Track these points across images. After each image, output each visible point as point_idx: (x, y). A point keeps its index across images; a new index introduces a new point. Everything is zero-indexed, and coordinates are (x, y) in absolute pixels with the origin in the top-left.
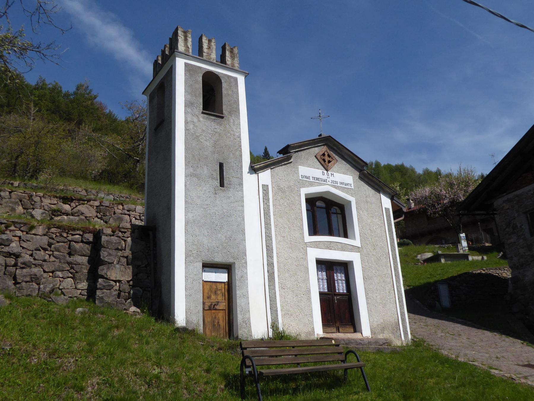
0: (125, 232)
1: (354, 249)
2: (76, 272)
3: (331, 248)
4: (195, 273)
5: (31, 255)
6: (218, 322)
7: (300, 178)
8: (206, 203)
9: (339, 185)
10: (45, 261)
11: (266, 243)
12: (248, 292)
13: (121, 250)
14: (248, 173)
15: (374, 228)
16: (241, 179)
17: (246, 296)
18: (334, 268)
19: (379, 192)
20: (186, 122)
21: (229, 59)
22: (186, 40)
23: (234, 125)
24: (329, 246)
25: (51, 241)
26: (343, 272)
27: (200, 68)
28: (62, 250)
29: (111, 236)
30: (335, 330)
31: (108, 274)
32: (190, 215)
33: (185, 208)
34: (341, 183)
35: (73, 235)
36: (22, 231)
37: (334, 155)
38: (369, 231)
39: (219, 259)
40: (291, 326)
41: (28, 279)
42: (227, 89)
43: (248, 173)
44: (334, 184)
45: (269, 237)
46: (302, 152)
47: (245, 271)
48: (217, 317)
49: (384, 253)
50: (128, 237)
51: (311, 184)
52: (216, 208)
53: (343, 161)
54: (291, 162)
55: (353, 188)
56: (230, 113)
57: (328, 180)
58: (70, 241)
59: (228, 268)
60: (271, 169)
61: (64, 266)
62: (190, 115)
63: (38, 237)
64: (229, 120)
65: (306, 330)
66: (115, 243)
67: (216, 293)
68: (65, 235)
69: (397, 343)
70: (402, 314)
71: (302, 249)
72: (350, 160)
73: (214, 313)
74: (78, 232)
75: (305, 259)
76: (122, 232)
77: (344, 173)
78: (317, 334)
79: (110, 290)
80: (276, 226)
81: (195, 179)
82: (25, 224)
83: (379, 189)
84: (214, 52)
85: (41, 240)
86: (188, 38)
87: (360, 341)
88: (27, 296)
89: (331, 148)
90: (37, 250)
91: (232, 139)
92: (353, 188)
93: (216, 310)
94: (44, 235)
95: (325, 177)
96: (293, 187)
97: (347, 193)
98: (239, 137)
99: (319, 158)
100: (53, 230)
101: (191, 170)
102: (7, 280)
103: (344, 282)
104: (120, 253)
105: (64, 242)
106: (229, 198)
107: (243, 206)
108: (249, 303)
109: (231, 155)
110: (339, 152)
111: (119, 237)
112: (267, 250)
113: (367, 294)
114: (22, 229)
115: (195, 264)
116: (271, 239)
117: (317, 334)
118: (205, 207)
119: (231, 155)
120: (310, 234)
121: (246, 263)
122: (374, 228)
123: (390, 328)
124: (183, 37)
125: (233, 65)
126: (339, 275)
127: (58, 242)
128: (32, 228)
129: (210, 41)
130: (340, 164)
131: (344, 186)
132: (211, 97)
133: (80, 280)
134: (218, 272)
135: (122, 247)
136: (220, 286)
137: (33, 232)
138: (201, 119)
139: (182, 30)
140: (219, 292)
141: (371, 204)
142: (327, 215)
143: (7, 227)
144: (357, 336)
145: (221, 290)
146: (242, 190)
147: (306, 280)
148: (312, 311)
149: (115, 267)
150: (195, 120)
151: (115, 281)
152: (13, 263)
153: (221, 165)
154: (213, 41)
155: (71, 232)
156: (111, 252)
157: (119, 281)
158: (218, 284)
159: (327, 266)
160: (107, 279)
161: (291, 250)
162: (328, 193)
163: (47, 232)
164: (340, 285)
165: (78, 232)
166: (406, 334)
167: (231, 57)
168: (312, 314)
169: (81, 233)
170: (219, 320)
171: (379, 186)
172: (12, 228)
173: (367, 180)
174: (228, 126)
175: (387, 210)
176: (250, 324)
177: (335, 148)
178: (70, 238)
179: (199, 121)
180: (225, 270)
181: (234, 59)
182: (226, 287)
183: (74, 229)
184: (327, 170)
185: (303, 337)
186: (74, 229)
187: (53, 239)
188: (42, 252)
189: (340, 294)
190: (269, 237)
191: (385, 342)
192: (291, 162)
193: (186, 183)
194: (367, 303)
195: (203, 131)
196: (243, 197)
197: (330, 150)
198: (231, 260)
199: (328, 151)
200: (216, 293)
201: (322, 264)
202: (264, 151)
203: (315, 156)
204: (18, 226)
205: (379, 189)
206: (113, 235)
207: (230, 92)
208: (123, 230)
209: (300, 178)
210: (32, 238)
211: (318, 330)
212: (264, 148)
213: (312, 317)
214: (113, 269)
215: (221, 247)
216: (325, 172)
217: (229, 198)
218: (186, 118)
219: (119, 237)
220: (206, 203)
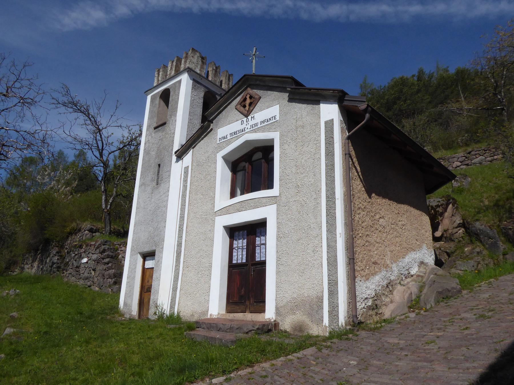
9: (259, 126)
22: (159, 74)
34: (263, 122)
44: (255, 129)
46: (224, 112)
51: (229, 142)
53: (269, 92)
72: (276, 85)
83: (318, 99)
98: (174, 133)
113: (278, 259)
117: (211, 315)
120: (270, 186)
122: (303, 161)
131: (266, 123)
173: (297, 97)
177: (258, 82)
184: (247, 116)
192: (212, 130)
201: (233, 231)
205: (318, 99)
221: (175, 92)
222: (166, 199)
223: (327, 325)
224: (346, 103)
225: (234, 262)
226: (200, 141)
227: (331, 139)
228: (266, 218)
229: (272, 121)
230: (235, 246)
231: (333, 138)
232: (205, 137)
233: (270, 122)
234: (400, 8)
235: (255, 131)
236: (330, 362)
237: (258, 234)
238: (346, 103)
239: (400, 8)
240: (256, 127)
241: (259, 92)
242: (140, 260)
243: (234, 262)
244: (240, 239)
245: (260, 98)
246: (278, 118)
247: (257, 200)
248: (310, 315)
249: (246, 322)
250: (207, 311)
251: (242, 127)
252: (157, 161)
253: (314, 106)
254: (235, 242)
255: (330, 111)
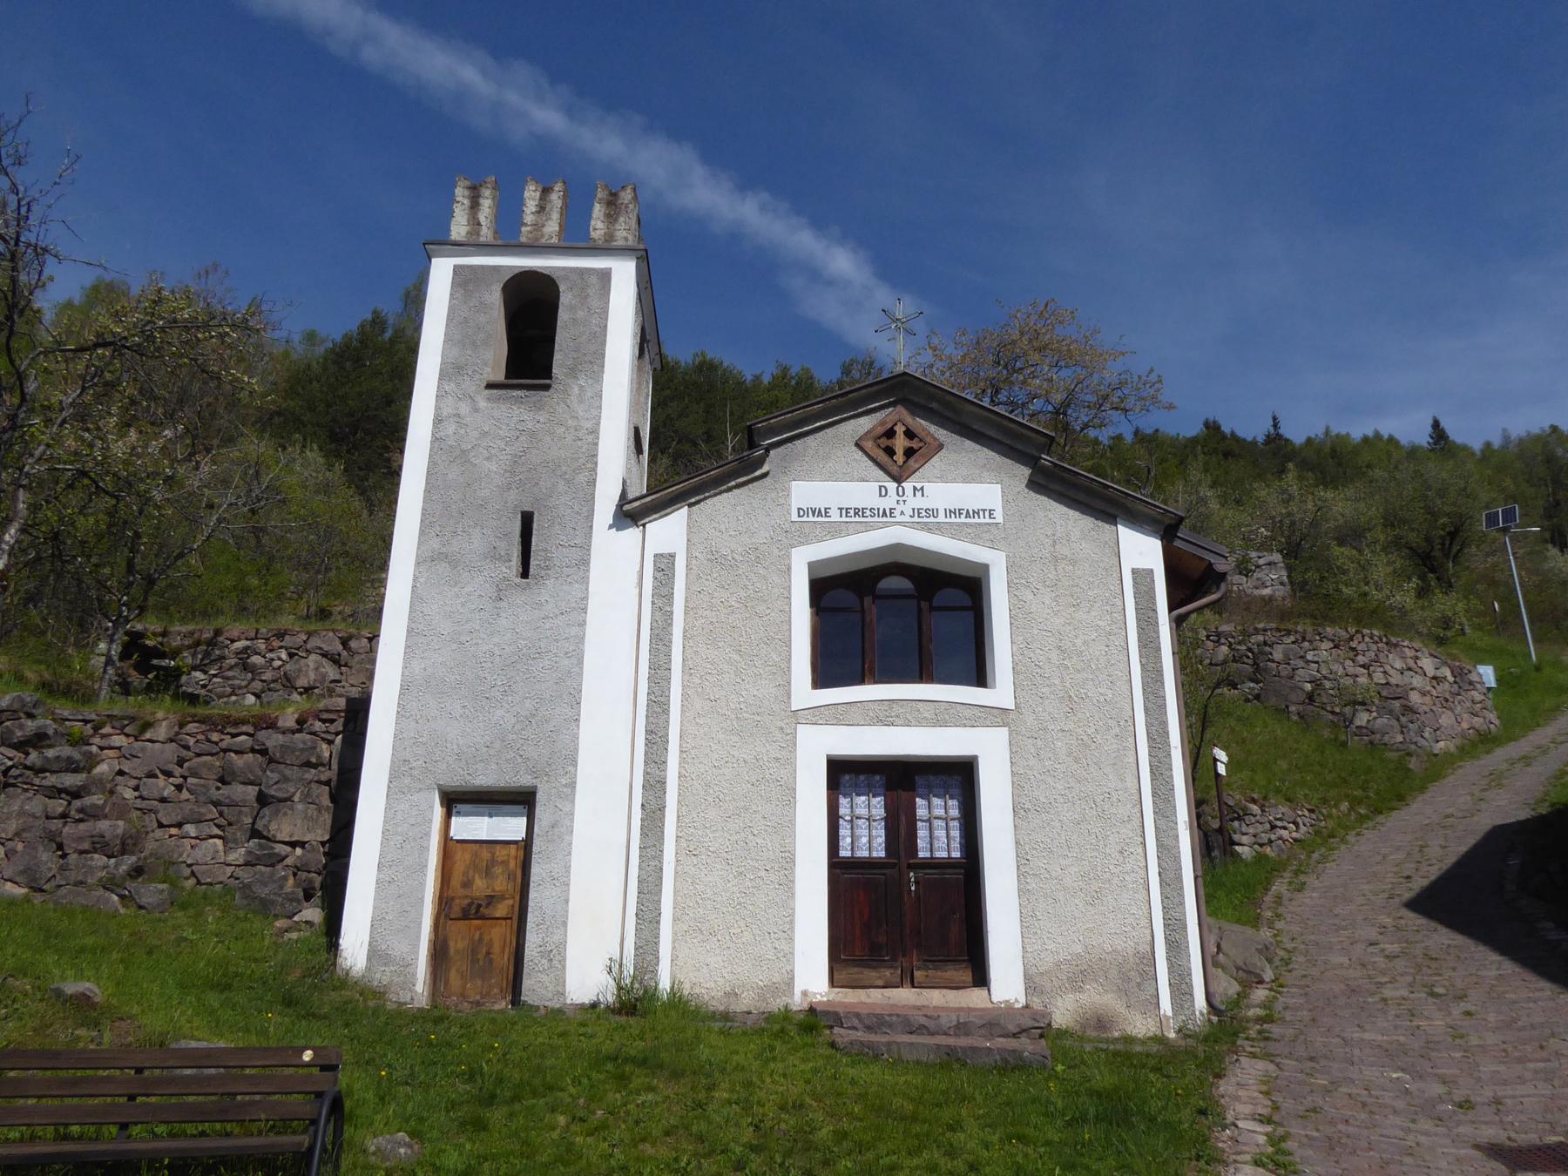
0: (332, 721)
1: (995, 716)
2: (230, 824)
3: (903, 720)
4: (412, 821)
5: (136, 789)
6: (488, 953)
7: (794, 517)
8: (467, 627)
9: (941, 518)
10: (163, 800)
11: (611, 728)
12: (568, 868)
13: (315, 766)
14: (611, 527)
15: (1079, 642)
16: (587, 548)
17: (562, 881)
18: (919, 780)
19: (1112, 519)
20: (438, 421)
21: (600, 225)
22: (475, 205)
23: (581, 402)
24: (885, 715)
25: (184, 753)
26: (957, 791)
27: (496, 269)
28: (204, 772)
29: (293, 732)
30: (967, 976)
31: (273, 826)
32: (417, 666)
33: (407, 647)
35: (234, 736)
36: (127, 735)
37: (933, 429)
38: (1054, 656)
39: (486, 778)
40: (689, 968)
41: (86, 846)
42: (572, 308)
43: (611, 527)
44: (925, 519)
45: (658, 706)
46: (810, 440)
47: (567, 809)
48: (486, 938)
49: (1112, 723)
50: (337, 734)
51: (835, 531)
52: (496, 640)
53: (968, 443)
54: (765, 475)
55: (999, 519)
56: (573, 372)
57: (900, 508)
58: (225, 751)
59: (523, 800)
60: (690, 505)
61: (202, 810)
62: (450, 400)
63: (157, 745)
64: (565, 392)
65: (761, 978)
66: (302, 750)
67: (488, 873)
68: (215, 737)
69: (1140, 1026)
70: (1174, 927)
71: (778, 735)
72: (992, 433)
73: (478, 928)
74: (244, 728)
75: (788, 760)
76: (324, 721)
77: (966, 480)
78: (805, 993)
79: (273, 865)
80: (687, 670)
81: (443, 567)
82: (133, 719)
83: (1112, 511)
84: (555, 216)
85: (162, 752)
86: (482, 201)
87: (923, 1021)
88: (75, 884)
89: (916, 409)
90: (152, 775)
91: (569, 438)
92: (999, 519)
93: (483, 918)
94: (172, 741)
95: (888, 503)
96: (762, 548)
97: (974, 540)
99: (869, 445)
100: (191, 728)
101: (435, 544)
102: (41, 848)
103: (956, 824)
104: (311, 774)
105: (212, 755)
106: (540, 604)
107: (583, 624)
108: (567, 901)
109: (561, 486)
110: (950, 415)
111: (314, 734)
112: (648, 742)
114: (127, 730)
115: (415, 798)
116: (666, 712)
117: (805, 993)
118: (463, 639)
119: (561, 486)
121: (572, 785)
122: (1079, 642)
123: (1113, 973)
124: (466, 202)
125: (610, 237)
126: (936, 801)
127: (199, 755)
128: (147, 726)
129: (546, 191)
130: (959, 451)
131: (963, 519)
132: (531, 336)
133: (235, 841)
134: (497, 815)
135: (319, 757)
136: (504, 852)
137: (148, 735)
138: (482, 404)
139: (467, 183)
140: (498, 870)
141: (1073, 562)
142: (899, 618)
143: (96, 729)
144: (973, 998)
145: (505, 863)
146: (585, 580)
147: (786, 827)
148: (792, 922)
149: (292, 808)
150: (464, 408)
151: (293, 845)
152: (60, 810)
153: (527, 520)
154: (558, 187)
155: (229, 730)
156: (288, 772)
157: (302, 844)
158: (498, 847)
159: (899, 779)
160: (268, 839)
161: (736, 738)
162: (897, 547)
163: (177, 734)
164: (940, 833)
165: (244, 728)
166: (1181, 989)
167: (608, 216)
168: (792, 929)
169: (250, 729)
170: (490, 945)
171: (1111, 501)
172: (107, 730)
173: (1057, 487)
174: (561, 408)
175: (1142, 578)
176: (563, 961)
177: (934, 405)
178: (228, 741)
179: (477, 410)
180: (519, 808)
181: (616, 220)
182: (521, 853)
183: (236, 723)
184: (898, 480)
185: (746, 1002)
186: (236, 723)
187: (187, 748)
188: (161, 780)
189: (933, 864)
190: (658, 706)
191: (1031, 1023)
192: (765, 475)
193: (415, 579)
194: (1022, 892)
195: (485, 434)
196: (585, 598)
197: (913, 414)
198: (525, 780)
199: (909, 420)
200: (488, 873)
201: (845, 774)
202: (1430, 430)
203: (857, 445)
204: (117, 724)
205: (1112, 511)
206: (300, 731)
207: (580, 314)
208: (325, 716)
209: (794, 517)
210: (143, 750)
211: (810, 976)
212: (1431, 422)
213: (791, 940)
214: (285, 814)
215: (498, 745)
216: (892, 486)
217: (540, 604)
218: (437, 408)
219: (314, 734)
220: (467, 627)
221: (584, 298)
222: (574, 631)
223: (1170, 1013)
224: (1177, 543)
225: (845, 853)
226: (720, 493)
227: (1151, 614)
228: (975, 758)
229: (982, 520)
230: (842, 811)
231: (1155, 611)
232: (738, 486)
233: (976, 520)
234: (512, 97)
235: (927, 528)
236: (913, 1100)
237: (920, 791)
238: (1177, 543)
239: (512, 97)
240: (932, 519)
241: (941, 434)
242: (438, 811)
243: (845, 853)
244: (858, 795)
245: (941, 447)
246: (999, 517)
247: (943, 707)
248: (1123, 992)
249: (932, 1014)
250: (790, 983)
251: (886, 503)
252: (517, 500)
253: (1100, 523)
254: (844, 802)
255: (1142, 551)
